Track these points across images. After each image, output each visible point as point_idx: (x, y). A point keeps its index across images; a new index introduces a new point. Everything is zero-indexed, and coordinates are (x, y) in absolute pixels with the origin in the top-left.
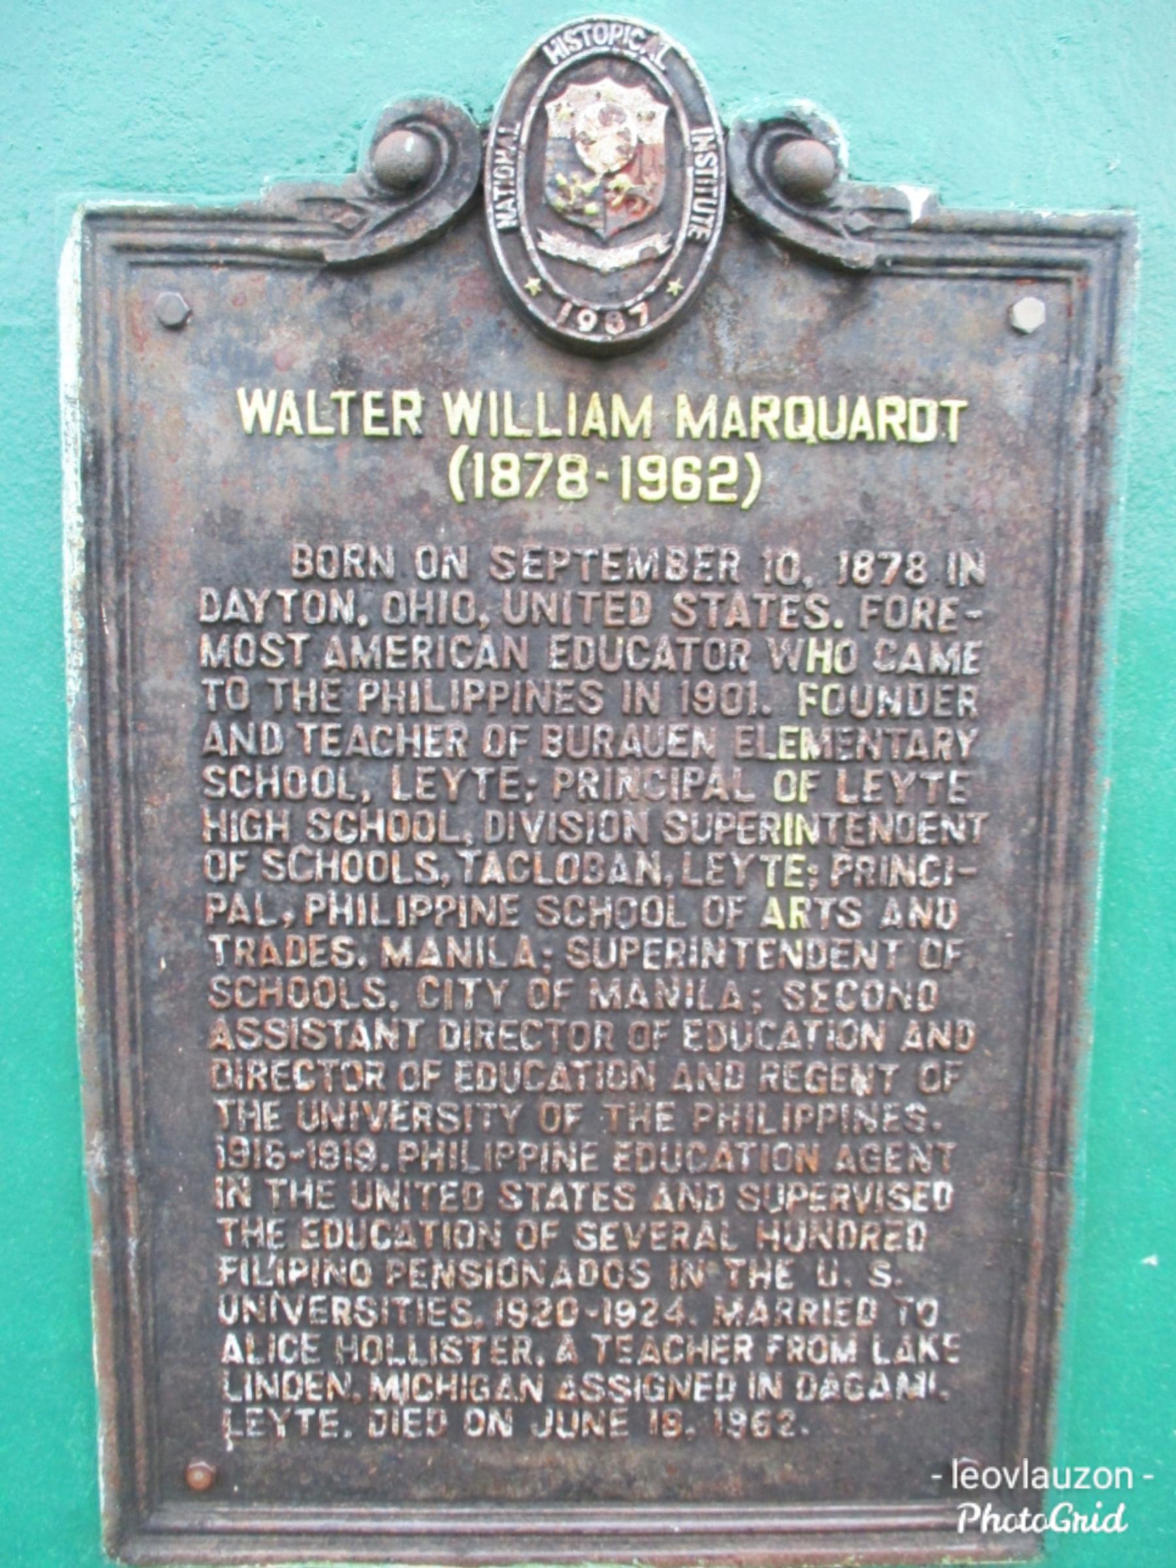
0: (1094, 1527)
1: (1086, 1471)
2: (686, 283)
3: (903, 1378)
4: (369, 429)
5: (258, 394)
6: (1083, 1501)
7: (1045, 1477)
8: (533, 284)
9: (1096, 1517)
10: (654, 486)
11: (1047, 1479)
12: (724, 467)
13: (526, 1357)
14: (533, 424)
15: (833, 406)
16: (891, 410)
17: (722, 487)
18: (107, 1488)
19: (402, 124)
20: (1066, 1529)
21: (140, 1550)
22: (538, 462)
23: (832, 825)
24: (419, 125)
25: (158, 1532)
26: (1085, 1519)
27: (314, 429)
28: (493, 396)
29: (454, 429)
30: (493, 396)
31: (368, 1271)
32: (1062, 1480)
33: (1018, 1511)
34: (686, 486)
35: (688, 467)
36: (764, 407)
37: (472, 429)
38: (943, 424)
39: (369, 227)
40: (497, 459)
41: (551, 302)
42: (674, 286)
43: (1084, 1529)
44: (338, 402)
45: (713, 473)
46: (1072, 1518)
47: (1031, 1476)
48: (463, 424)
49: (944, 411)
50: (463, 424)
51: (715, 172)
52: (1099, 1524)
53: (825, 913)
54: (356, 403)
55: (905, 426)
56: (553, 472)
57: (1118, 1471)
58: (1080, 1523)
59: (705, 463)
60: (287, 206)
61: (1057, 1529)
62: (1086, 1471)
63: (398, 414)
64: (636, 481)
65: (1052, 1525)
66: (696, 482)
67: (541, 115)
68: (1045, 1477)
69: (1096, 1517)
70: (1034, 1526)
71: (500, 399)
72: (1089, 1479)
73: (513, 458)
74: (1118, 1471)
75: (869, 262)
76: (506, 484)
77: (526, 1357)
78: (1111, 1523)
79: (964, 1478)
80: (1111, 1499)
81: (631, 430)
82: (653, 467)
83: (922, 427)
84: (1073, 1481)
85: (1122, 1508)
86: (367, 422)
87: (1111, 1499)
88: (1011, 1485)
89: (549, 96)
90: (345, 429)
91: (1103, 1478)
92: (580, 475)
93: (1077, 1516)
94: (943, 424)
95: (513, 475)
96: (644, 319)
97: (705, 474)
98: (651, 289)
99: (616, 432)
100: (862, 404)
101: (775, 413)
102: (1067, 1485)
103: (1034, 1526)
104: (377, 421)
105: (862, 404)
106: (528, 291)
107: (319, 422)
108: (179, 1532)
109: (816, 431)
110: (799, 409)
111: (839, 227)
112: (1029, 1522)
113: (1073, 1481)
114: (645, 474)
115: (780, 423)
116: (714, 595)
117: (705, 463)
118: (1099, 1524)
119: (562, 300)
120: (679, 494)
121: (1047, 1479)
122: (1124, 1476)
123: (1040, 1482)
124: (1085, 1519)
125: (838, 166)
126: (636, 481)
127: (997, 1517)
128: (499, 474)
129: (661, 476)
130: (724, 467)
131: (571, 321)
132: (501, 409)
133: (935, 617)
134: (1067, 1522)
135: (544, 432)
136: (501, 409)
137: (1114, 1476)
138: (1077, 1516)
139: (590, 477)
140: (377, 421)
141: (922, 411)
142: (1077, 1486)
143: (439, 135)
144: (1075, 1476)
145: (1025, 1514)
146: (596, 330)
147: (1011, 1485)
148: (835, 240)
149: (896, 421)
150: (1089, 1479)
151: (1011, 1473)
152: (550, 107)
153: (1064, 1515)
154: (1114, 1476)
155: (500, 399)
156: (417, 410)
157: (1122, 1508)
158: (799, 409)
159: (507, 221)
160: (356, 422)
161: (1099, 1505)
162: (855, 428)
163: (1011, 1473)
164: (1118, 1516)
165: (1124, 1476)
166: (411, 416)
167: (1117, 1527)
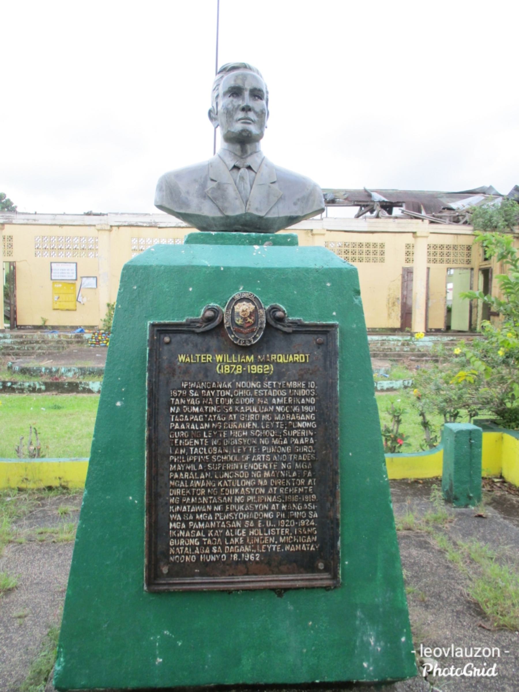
0: (483, 674)
3: (181, 474)
4: (202, 361)
5: (182, 355)
10: (254, 371)
12: (266, 367)
14: (232, 360)
16: (296, 357)
17: (267, 371)
18: (146, 571)
19: (209, 309)
20: (471, 675)
26: (479, 670)
29: (218, 361)
31: (195, 558)
32: (468, 653)
33: (450, 666)
36: (273, 357)
37: (221, 361)
40: (225, 366)
43: (479, 675)
47: (455, 652)
48: (219, 360)
50: (219, 360)
52: (485, 672)
53: (263, 458)
56: (236, 369)
63: (208, 358)
64: (251, 370)
66: (261, 370)
68: (461, 652)
69: (484, 670)
70: (456, 674)
72: (480, 653)
73: (228, 366)
76: (227, 371)
78: (490, 672)
84: (474, 654)
85: (495, 665)
87: (490, 662)
88: (446, 655)
92: (240, 369)
93: (475, 669)
95: (228, 369)
97: (263, 368)
100: (291, 356)
101: (275, 358)
102: (471, 656)
104: (204, 360)
105: (291, 356)
113: (474, 654)
114: (252, 369)
115: (276, 359)
118: (485, 672)
120: (258, 372)
122: (496, 651)
123: (459, 654)
124: (479, 670)
126: (251, 370)
127: (440, 670)
128: (226, 369)
130: (266, 367)
131: (240, 342)
133: (181, 493)
134: (471, 672)
139: (242, 369)
140: (204, 360)
145: (452, 668)
147: (446, 655)
149: (297, 359)
150: (480, 653)
153: (469, 668)
156: (211, 358)
159: (228, 326)
162: (290, 360)
164: (493, 669)
165: (496, 651)
166: (210, 359)
167: (493, 674)
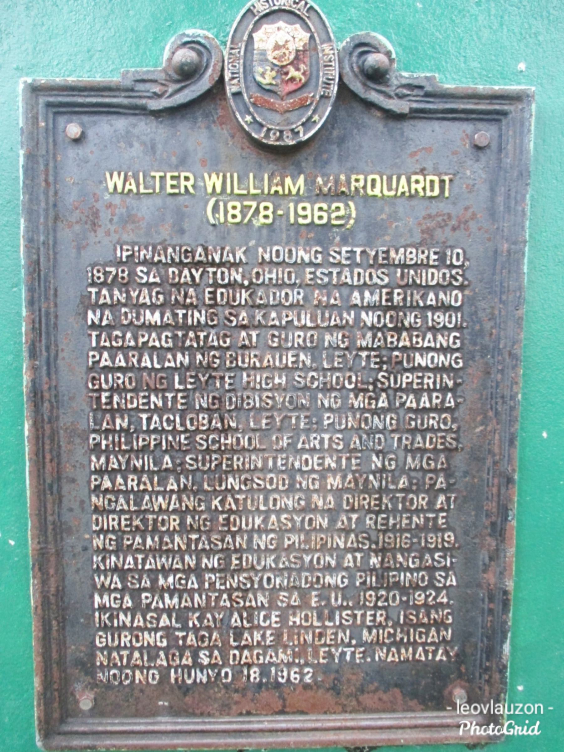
0: (525, 732)
1: (521, 705)
2: (321, 118)
6: (519, 720)
7: (501, 709)
8: (249, 118)
9: (525, 728)
10: (305, 217)
11: (502, 709)
12: (338, 209)
13: (301, 343)
14: (248, 189)
15: (390, 179)
17: (338, 218)
20: (511, 733)
21: (59, 741)
22: (250, 207)
23: (359, 618)
24: (193, 45)
25: (66, 733)
26: (520, 728)
27: (142, 190)
28: (228, 175)
30: (228, 175)
31: (157, 677)
33: (488, 725)
34: (320, 218)
35: (320, 209)
38: (442, 189)
39: (168, 94)
41: (256, 126)
42: (316, 118)
43: (520, 733)
44: (154, 177)
45: (333, 211)
46: (514, 728)
47: (494, 708)
49: (442, 182)
51: (333, 64)
52: (527, 731)
54: (162, 178)
55: (424, 189)
57: (536, 706)
58: (518, 731)
59: (329, 207)
60: (128, 83)
61: (506, 733)
62: (521, 705)
65: (505, 731)
66: (325, 215)
67: (250, 37)
69: (525, 728)
70: (496, 732)
71: (232, 177)
72: (522, 710)
73: (238, 204)
74: (536, 706)
75: (406, 110)
76: (234, 216)
77: (301, 343)
78: (533, 730)
79: (462, 708)
80: (533, 719)
81: (294, 191)
82: (304, 209)
83: (432, 190)
84: (515, 711)
85: (538, 723)
86: (168, 187)
87: (533, 719)
89: (254, 30)
90: (157, 190)
91: (529, 709)
93: (516, 727)
94: (442, 189)
95: (237, 212)
96: (301, 134)
98: (304, 120)
99: (287, 192)
101: (362, 183)
103: (496, 732)
106: (246, 122)
107: (145, 188)
108: (77, 733)
109: (382, 192)
110: (373, 181)
111: (392, 94)
112: (493, 730)
113: (515, 711)
114: (301, 212)
115: (365, 187)
116: (335, 271)
117: (329, 207)
118: (527, 731)
119: (262, 126)
121: (502, 709)
122: (539, 708)
124: (520, 728)
125: (391, 61)
128: (231, 212)
129: (308, 212)
130: (338, 209)
132: (232, 182)
134: (512, 730)
135: (253, 191)
136: (232, 182)
137: (534, 708)
138: (516, 727)
141: (432, 182)
142: (517, 713)
143: (202, 50)
144: (516, 708)
145: (492, 726)
146: (278, 140)
148: (391, 101)
149: (420, 187)
150: (522, 710)
151: (485, 707)
152: (254, 35)
154: (534, 708)
155: (232, 177)
157: (538, 723)
158: (373, 181)
159: (235, 89)
160: (163, 187)
161: (527, 722)
162: (400, 190)
163: (485, 707)
164: (536, 727)
165: (539, 708)
167: (536, 732)
